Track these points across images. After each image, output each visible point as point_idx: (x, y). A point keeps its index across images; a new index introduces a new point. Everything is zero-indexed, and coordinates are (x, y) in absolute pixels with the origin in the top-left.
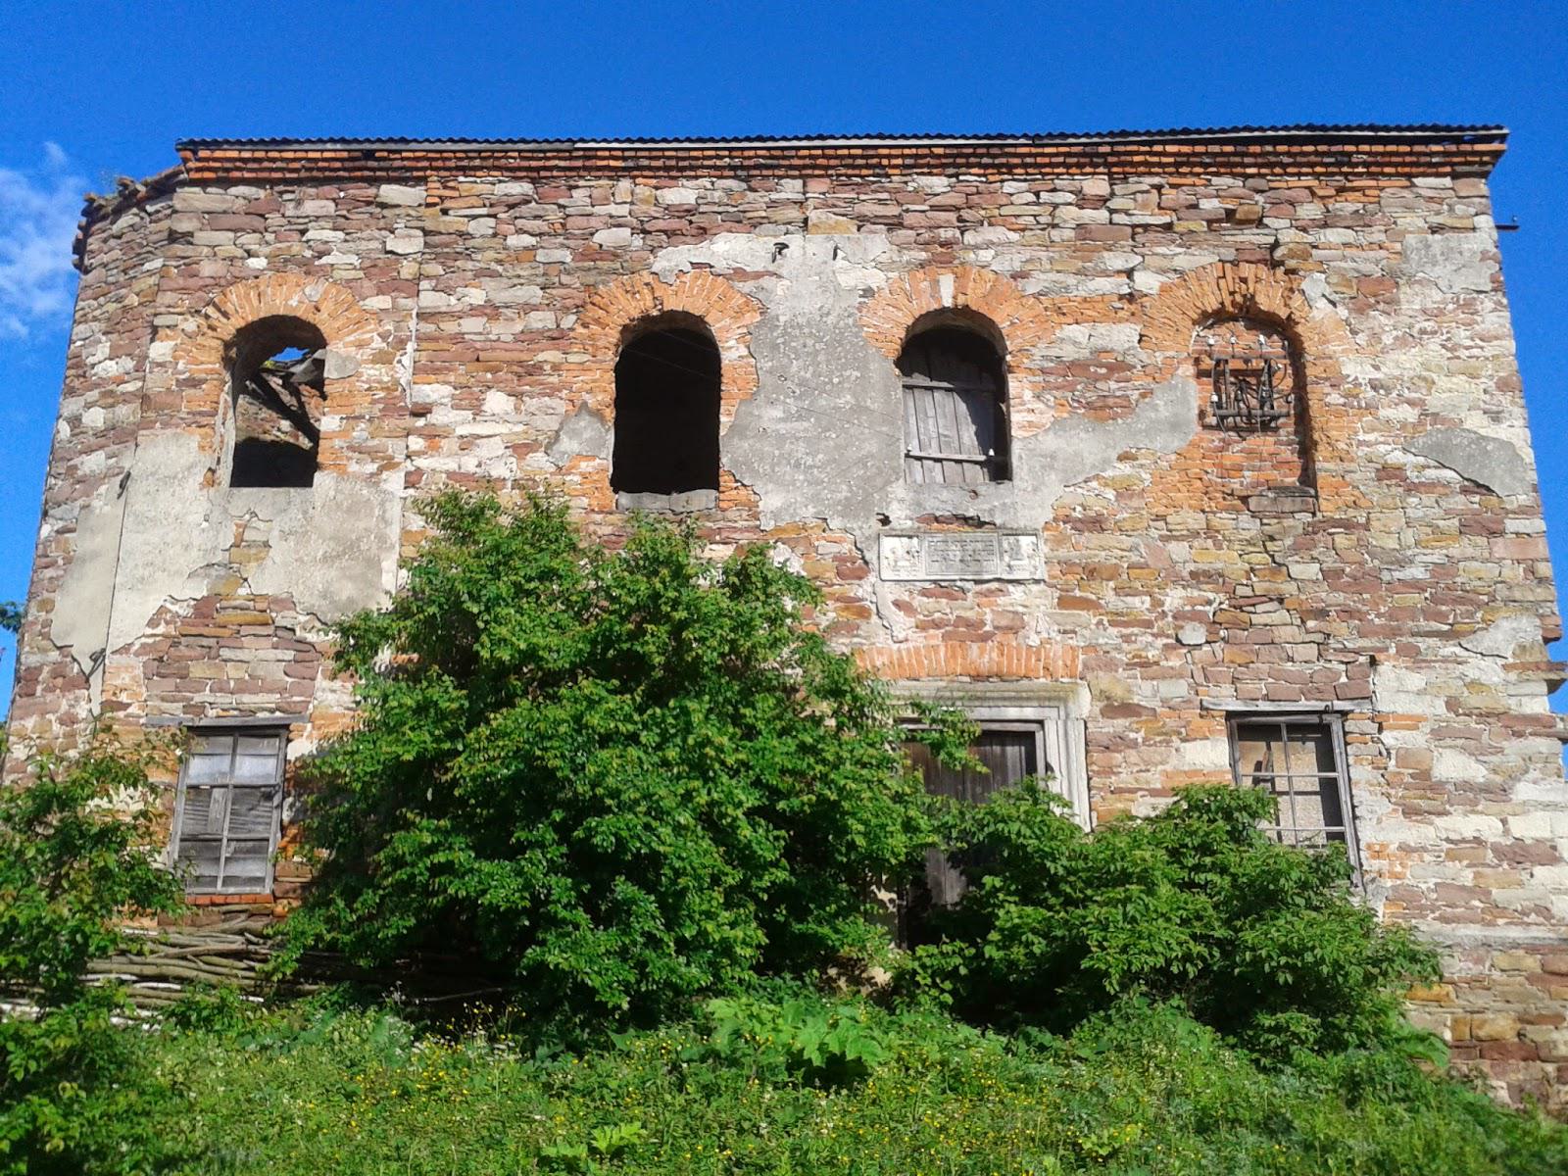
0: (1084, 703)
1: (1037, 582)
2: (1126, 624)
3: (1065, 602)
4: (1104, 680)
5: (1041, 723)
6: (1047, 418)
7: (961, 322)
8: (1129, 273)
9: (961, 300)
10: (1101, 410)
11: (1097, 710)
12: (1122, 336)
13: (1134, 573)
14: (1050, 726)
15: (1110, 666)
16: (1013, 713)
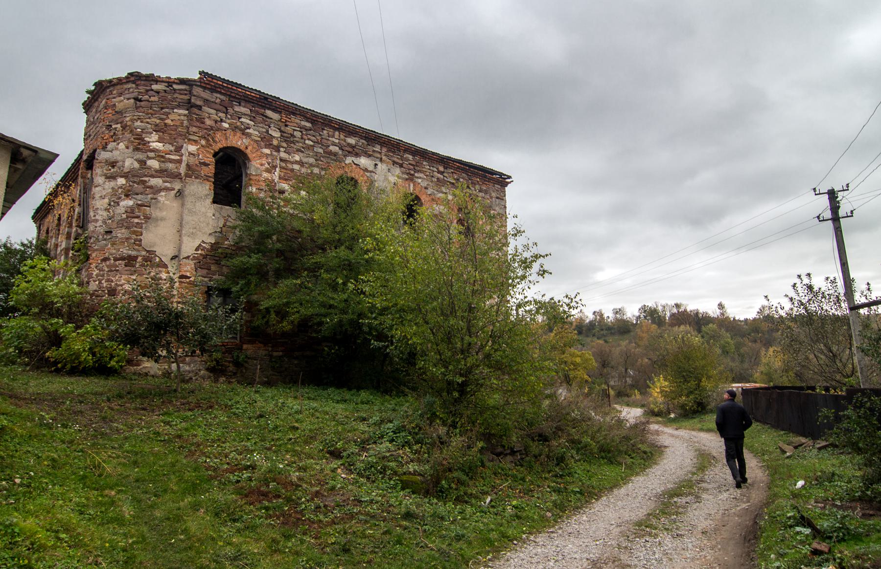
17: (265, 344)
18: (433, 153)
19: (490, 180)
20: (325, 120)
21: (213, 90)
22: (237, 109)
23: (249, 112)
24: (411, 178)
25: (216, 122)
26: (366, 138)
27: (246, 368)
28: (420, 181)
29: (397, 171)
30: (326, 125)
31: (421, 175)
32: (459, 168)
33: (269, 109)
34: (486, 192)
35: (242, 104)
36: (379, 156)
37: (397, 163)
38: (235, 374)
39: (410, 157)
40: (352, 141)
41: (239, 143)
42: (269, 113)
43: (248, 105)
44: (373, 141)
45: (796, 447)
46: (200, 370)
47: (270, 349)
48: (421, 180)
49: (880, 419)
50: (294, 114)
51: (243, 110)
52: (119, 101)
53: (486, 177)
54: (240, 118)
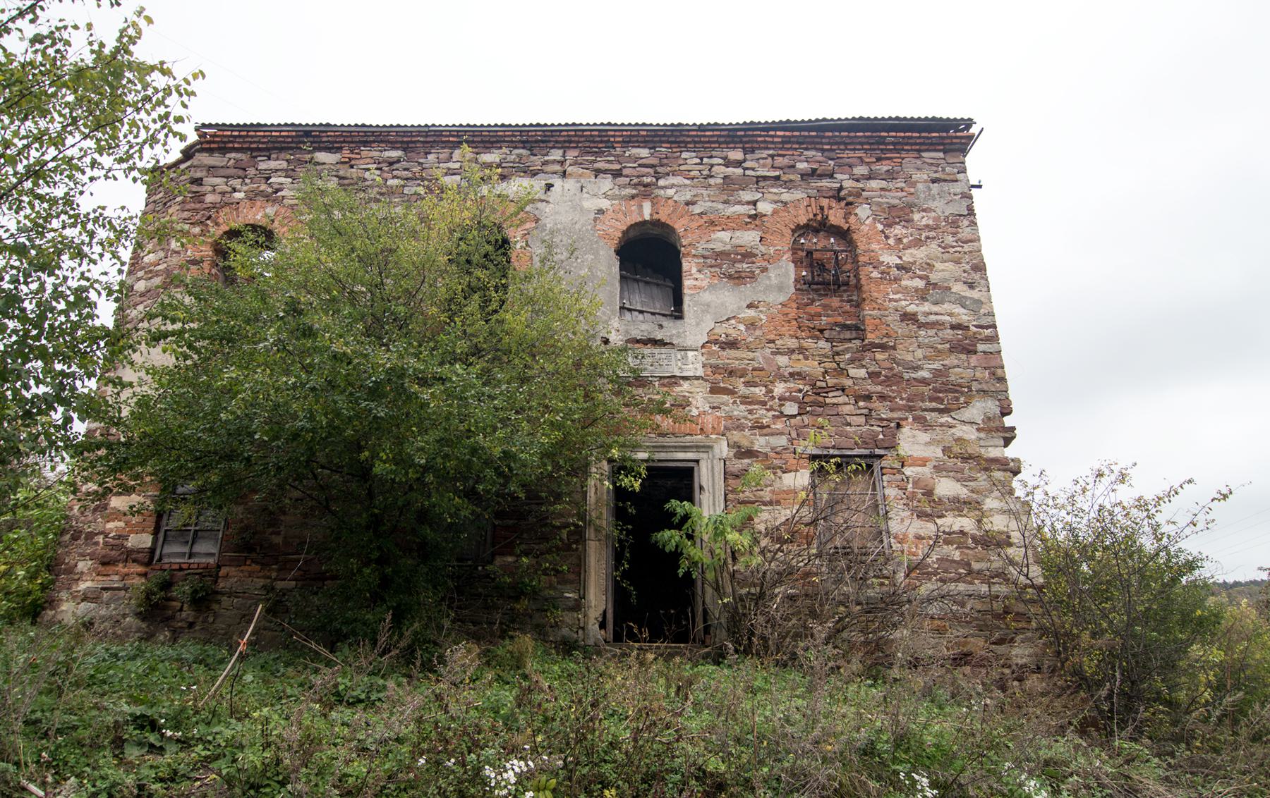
0: (723, 449)
1: (697, 378)
2: (750, 403)
3: (715, 390)
4: (736, 436)
5: (697, 461)
6: (705, 283)
7: (656, 231)
8: (754, 203)
9: (656, 217)
10: (738, 279)
11: (732, 454)
12: (749, 238)
13: (755, 373)
14: (702, 464)
15: (740, 428)
16: (681, 455)
17: (264, 565)
18: (701, 128)
19: (898, 146)
20: (427, 134)
21: (223, 150)
22: (262, 166)
23: (284, 165)
24: (646, 191)
25: (223, 193)
26: (524, 144)
27: (216, 615)
28: (670, 192)
29: (606, 183)
30: (433, 144)
31: (672, 180)
32: (786, 141)
33: (320, 149)
34: (891, 176)
35: (273, 156)
36: (557, 167)
37: (605, 172)
38: (191, 625)
39: (644, 152)
40: (491, 157)
41: (258, 217)
42: (321, 156)
43: (282, 155)
44: (535, 143)
45: (244, 169)
46: (124, 616)
47: (274, 575)
48: (674, 189)
49: (21, 91)
50: (366, 143)
51: (273, 164)
52: (1203, 770)
53: (882, 141)
54: (268, 179)
